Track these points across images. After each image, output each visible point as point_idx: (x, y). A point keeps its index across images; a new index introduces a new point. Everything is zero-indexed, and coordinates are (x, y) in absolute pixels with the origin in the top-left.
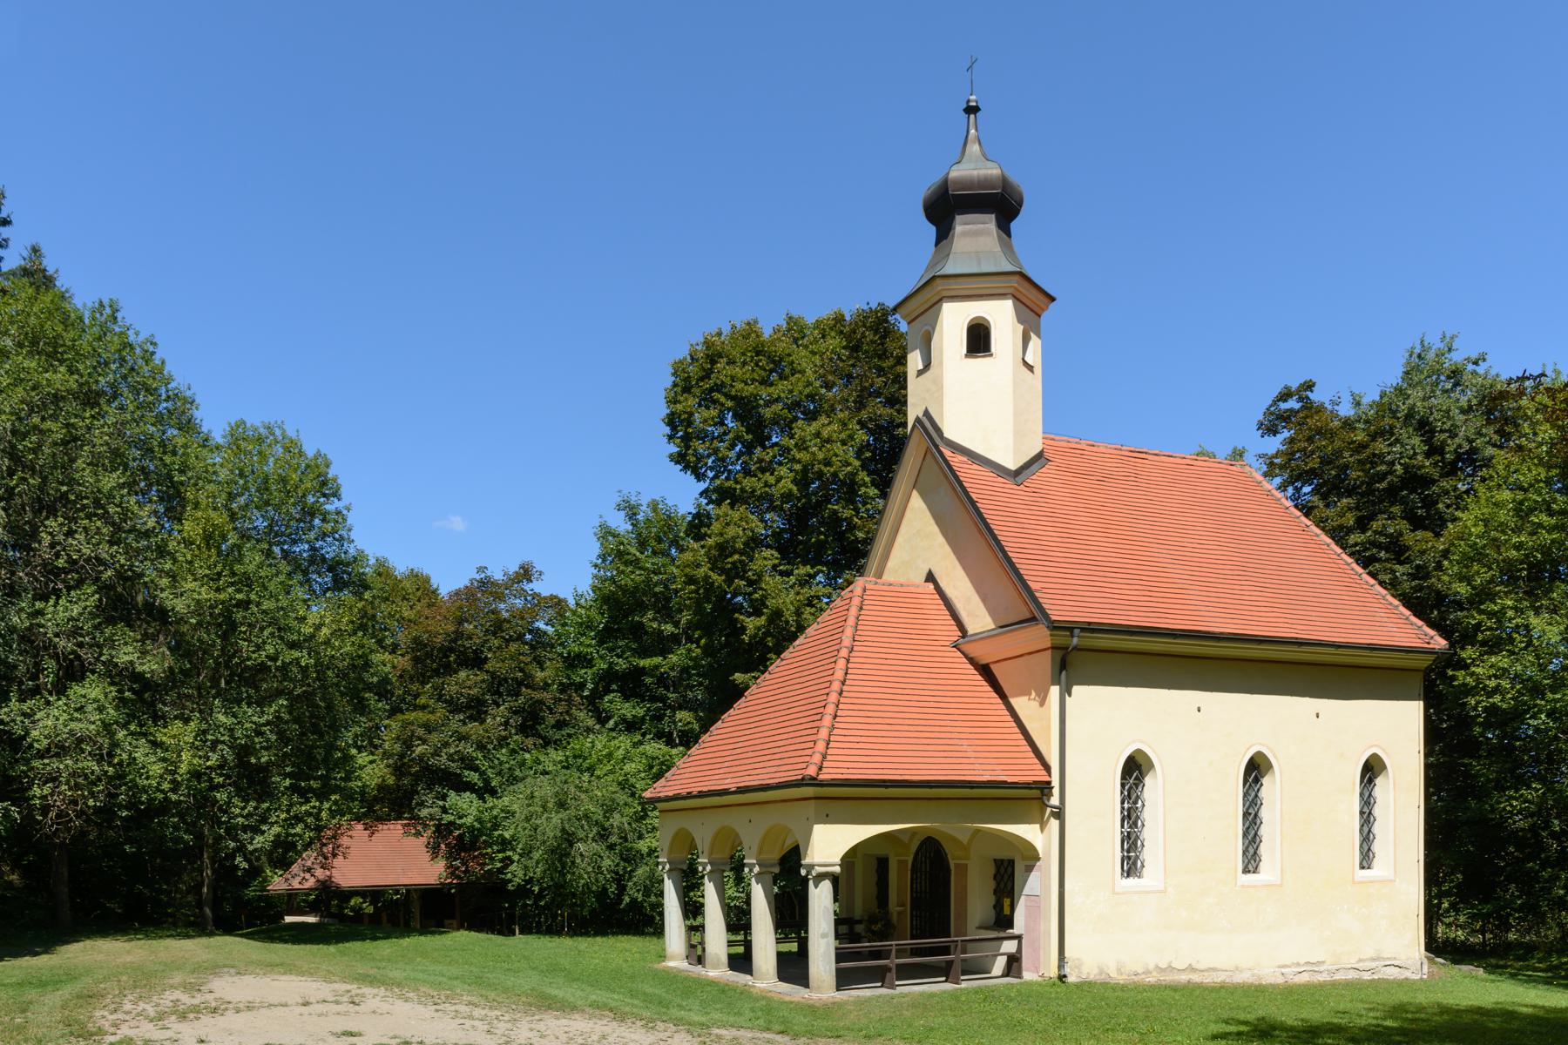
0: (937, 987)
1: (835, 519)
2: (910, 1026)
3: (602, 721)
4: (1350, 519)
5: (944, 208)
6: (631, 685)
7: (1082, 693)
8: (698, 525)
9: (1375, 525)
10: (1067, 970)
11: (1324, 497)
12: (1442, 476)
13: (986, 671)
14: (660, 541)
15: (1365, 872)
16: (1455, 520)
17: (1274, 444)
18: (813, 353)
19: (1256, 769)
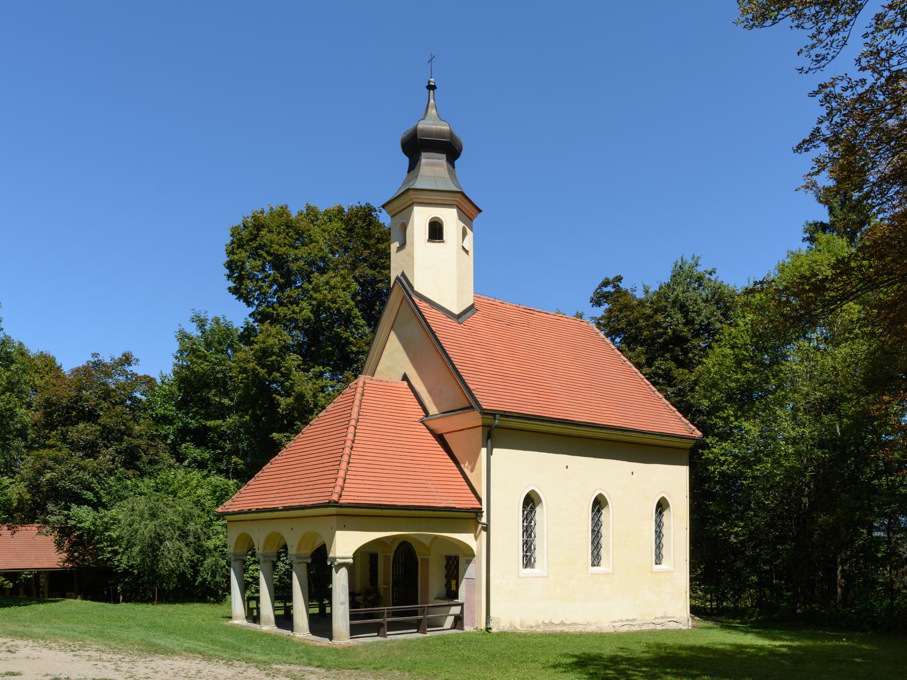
0: (413, 636)
1: (338, 336)
2: (401, 661)
3: (181, 460)
4: (643, 360)
5: (415, 146)
6: (201, 437)
7: (499, 453)
8: (247, 336)
9: (657, 363)
10: (491, 625)
12: (693, 337)
13: (440, 438)
14: (221, 344)
16: (700, 363)
17: (600, 311)
18: (324, 231)
19: (599, 504)
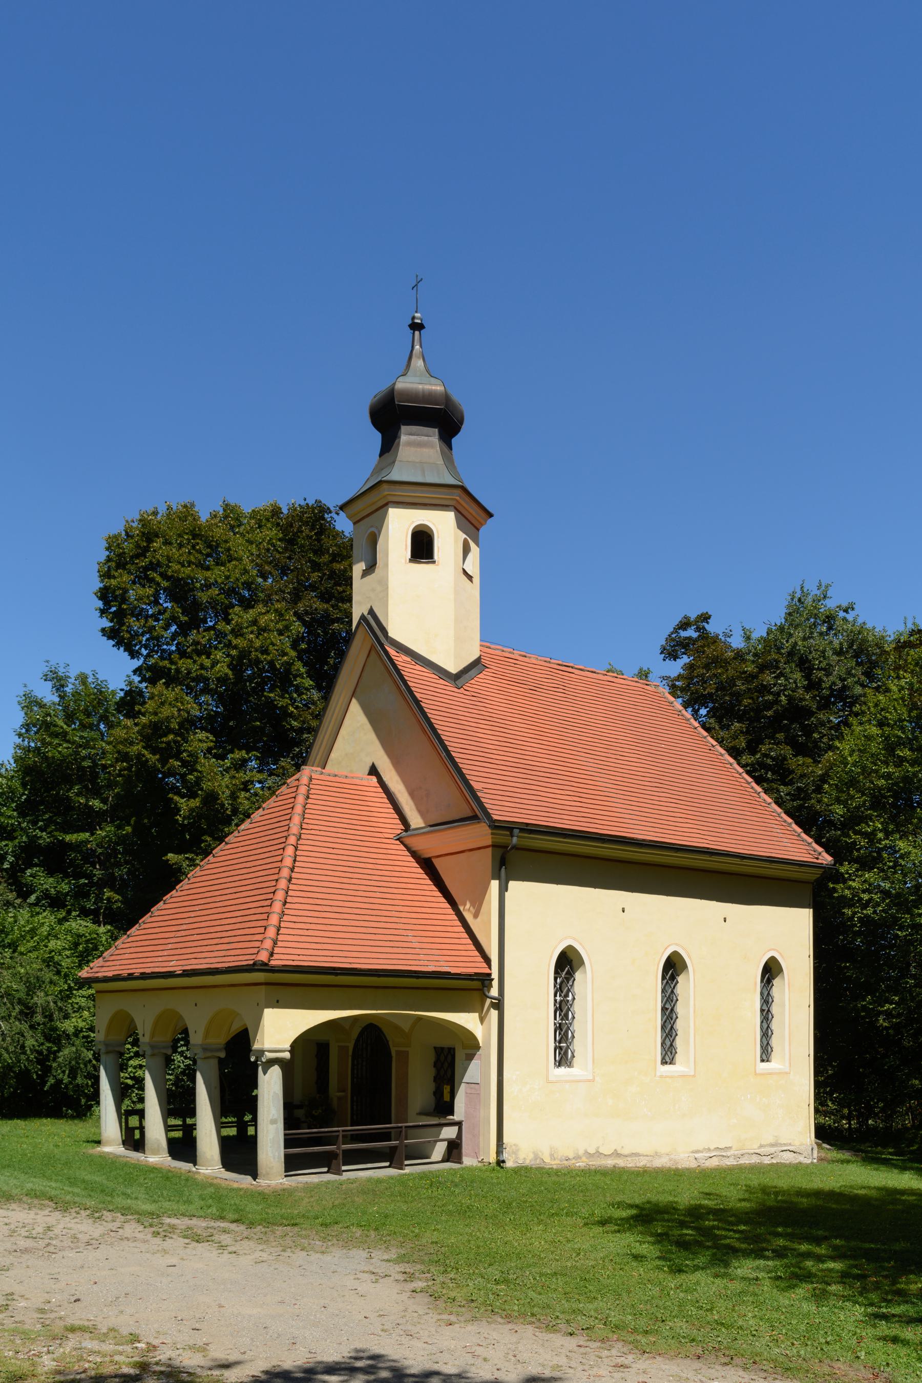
0: (382, 1172)
5: (392, 416)
6: (55, 859)
8: (131, 702)
9: (764, 748)
10: (505, 1156)
11: (719, 720)
12: (819, 709)
13: (427, 865)
14: (89, 715)
15: (668, 1068)
16: (831, 748)
17: (676, 668)
18: (250, 542)
19: (673, 967)
